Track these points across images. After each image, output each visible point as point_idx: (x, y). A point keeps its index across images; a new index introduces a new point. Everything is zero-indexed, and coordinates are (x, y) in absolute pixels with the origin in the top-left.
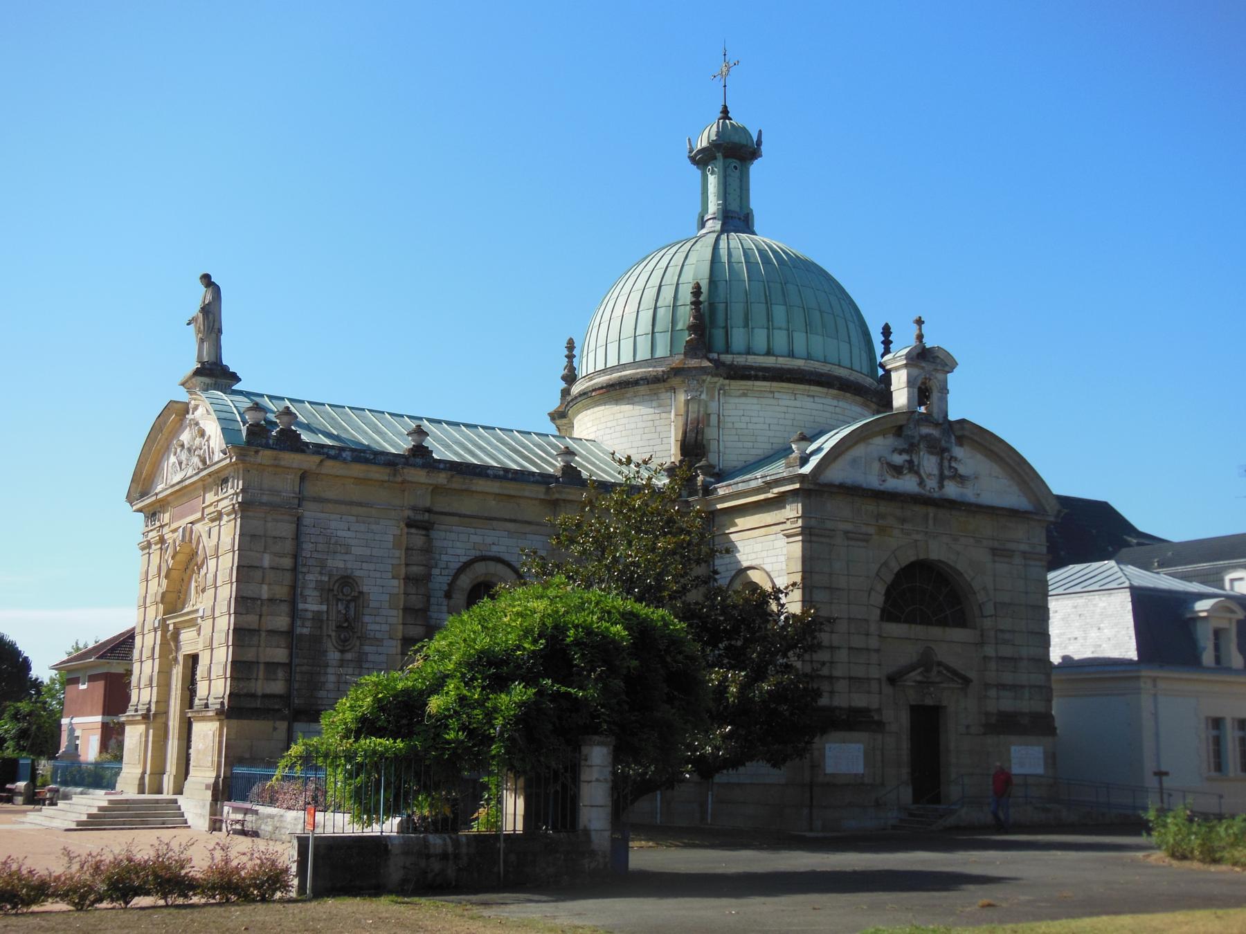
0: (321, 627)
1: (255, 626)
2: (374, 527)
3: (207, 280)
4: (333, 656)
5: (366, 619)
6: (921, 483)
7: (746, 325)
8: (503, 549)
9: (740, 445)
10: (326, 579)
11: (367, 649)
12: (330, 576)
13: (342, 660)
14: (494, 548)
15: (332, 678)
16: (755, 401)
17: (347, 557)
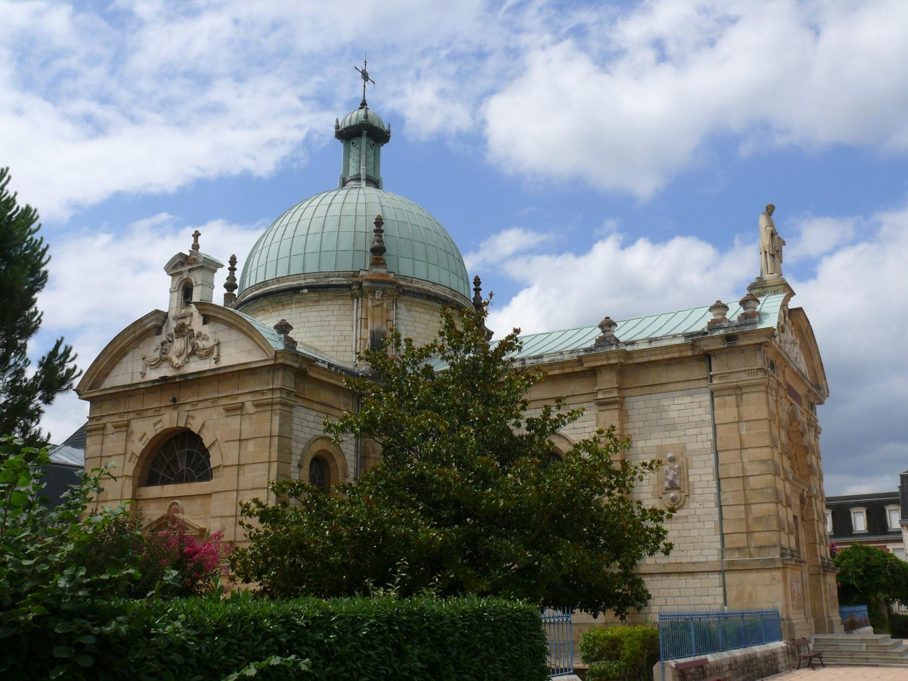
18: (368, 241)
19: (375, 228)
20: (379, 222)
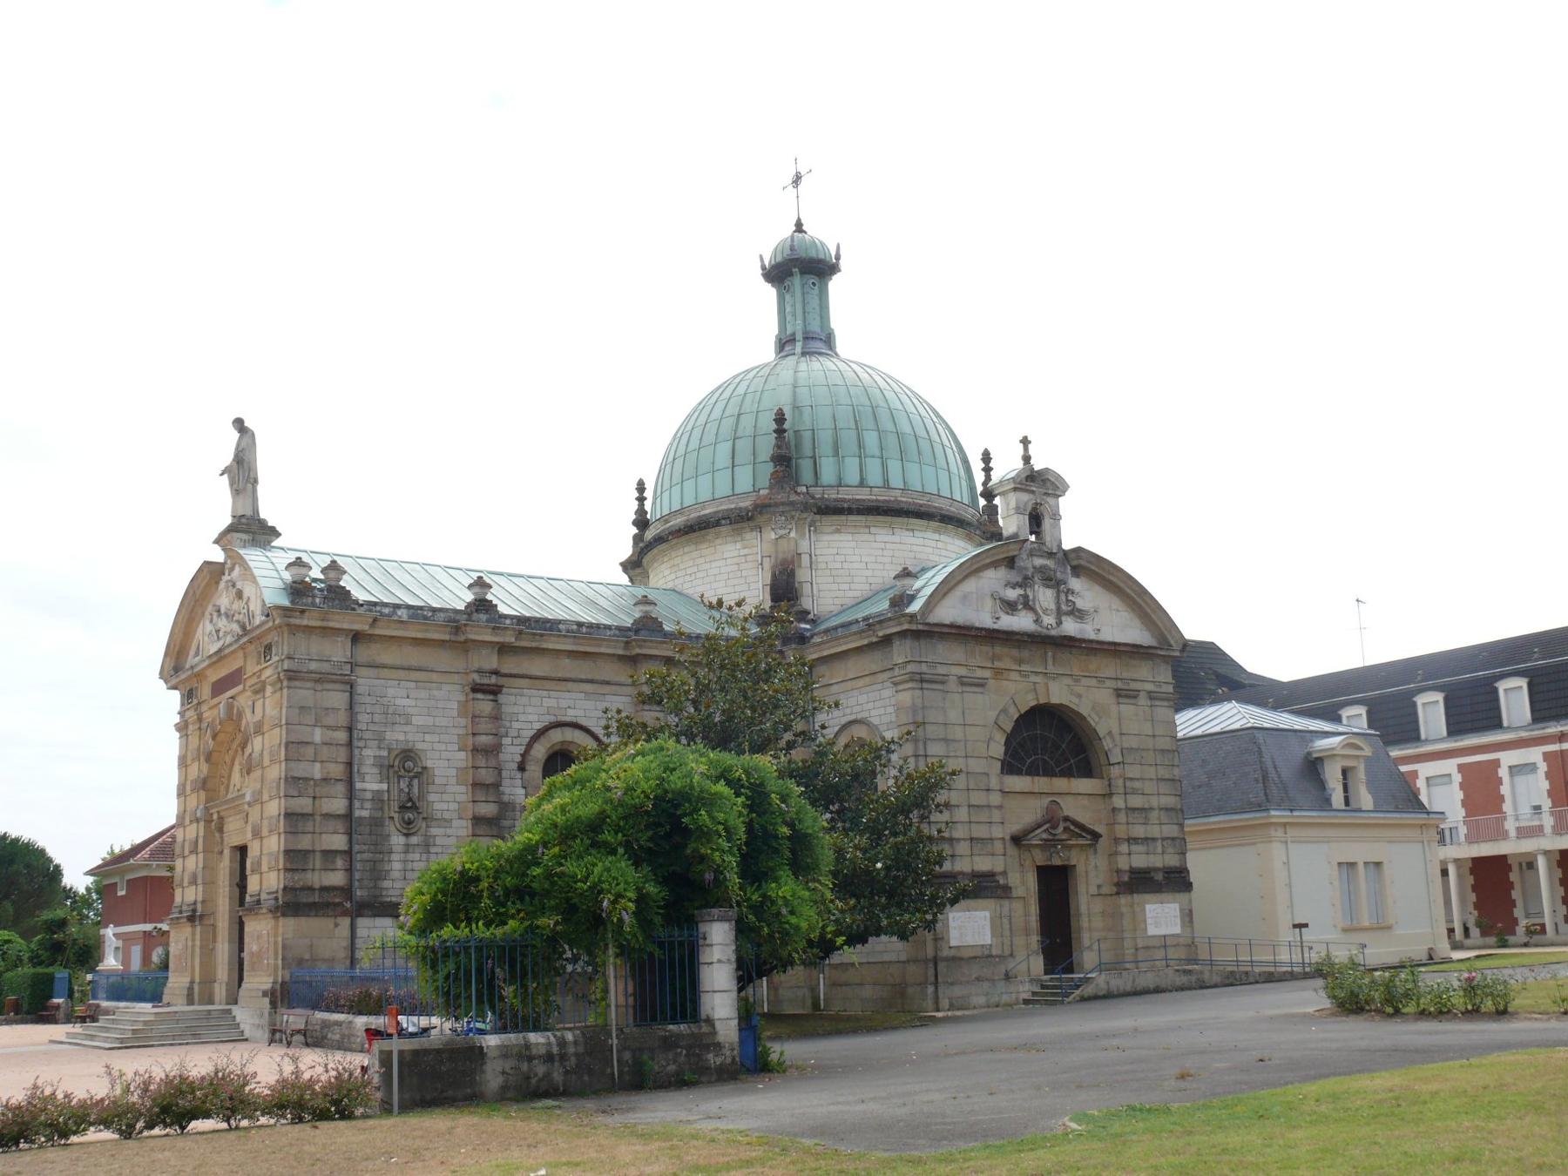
0: (382, 809)
1: (308, 810)
2: (436, 693)
3: (239, 424)
4: (397, 840)
5: (432, 797)
6: (1037, 621)
7: (836, 453)
8: (581, 713)
9: (835, 587)
10: (385, 753)
11: (434, 831)
12: (390, 750)
13: (407, 845)
14: (571, 712)
15: (397, 866)
16: (849, 537)
17: (407, 728)
18: (767, 446)
19: (775, 426)
20: (780, 418)
